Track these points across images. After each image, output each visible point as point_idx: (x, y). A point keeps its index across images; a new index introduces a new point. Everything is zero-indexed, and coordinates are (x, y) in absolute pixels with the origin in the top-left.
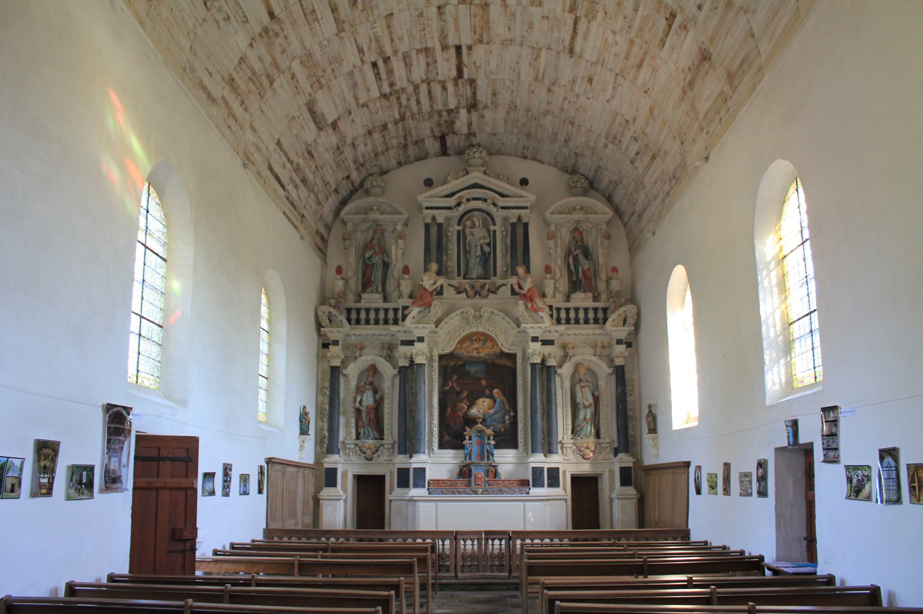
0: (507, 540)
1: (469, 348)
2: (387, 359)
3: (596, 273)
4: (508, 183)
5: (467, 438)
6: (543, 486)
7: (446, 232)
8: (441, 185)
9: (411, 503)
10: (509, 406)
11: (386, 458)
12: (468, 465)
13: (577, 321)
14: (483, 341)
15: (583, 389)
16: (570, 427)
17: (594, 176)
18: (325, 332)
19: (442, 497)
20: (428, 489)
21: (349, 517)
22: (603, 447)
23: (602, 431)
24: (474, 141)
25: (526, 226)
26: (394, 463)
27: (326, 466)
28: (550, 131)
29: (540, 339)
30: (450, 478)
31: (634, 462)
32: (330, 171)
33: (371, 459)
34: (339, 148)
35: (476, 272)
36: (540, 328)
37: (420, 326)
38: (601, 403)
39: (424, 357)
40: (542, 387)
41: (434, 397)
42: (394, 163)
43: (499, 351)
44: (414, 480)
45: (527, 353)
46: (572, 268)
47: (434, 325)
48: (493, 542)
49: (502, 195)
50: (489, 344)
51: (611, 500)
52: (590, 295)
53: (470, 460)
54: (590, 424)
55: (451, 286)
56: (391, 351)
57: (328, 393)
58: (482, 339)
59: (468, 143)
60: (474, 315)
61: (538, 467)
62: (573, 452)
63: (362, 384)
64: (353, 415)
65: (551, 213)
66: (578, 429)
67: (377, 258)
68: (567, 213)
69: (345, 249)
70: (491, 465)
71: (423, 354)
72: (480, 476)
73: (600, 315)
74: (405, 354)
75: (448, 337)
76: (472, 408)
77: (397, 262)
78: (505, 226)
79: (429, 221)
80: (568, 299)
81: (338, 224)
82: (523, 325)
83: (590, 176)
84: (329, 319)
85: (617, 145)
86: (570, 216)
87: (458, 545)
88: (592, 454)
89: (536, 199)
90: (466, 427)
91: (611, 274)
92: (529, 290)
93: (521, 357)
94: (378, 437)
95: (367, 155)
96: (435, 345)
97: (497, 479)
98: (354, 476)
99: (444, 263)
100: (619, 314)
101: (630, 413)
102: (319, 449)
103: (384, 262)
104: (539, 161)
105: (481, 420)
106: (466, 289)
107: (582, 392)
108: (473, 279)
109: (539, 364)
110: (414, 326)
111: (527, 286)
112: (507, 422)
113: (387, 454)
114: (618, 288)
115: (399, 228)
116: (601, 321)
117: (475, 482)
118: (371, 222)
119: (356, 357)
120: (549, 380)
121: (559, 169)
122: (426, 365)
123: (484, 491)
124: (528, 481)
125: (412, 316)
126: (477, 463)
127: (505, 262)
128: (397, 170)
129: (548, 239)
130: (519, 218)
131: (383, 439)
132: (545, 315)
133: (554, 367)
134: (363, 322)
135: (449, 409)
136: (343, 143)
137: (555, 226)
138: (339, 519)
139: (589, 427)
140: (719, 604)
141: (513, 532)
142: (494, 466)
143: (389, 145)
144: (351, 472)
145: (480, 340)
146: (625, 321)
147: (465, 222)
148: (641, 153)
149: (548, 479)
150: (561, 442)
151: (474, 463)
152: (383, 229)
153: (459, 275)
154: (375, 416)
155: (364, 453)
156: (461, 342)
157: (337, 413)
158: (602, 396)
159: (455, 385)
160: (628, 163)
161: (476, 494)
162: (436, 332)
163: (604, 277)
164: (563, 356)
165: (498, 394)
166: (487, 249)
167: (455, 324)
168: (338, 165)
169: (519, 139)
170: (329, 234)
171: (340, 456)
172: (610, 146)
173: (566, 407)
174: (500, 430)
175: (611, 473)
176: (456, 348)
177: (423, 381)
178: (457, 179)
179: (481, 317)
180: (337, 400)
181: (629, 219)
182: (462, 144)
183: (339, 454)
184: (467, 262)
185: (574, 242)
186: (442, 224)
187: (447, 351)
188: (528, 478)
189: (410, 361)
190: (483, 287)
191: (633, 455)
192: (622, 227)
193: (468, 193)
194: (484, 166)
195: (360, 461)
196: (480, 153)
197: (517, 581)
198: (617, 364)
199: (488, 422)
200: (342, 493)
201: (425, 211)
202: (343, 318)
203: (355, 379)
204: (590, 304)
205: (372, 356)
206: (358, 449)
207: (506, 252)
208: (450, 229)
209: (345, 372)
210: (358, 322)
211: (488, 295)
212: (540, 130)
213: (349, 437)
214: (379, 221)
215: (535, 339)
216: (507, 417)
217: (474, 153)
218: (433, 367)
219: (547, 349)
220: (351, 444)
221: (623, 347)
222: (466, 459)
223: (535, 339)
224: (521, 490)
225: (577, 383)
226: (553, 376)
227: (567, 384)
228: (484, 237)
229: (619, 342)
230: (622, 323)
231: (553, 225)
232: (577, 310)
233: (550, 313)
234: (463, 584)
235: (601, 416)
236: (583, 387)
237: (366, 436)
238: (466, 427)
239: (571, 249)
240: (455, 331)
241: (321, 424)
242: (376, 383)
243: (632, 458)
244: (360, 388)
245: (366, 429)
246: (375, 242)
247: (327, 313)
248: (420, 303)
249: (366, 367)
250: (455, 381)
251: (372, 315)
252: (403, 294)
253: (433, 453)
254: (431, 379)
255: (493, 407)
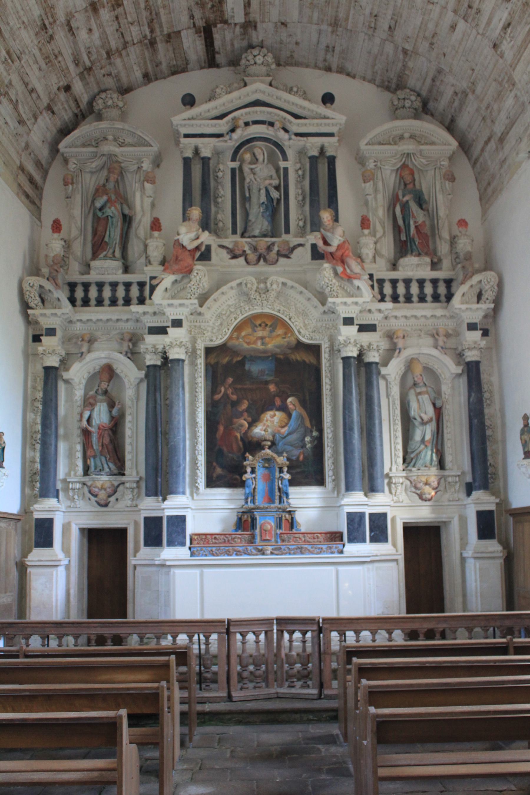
0: (316, 633)
1: (251, 337)
2: (129, 355)
3: (434, 228)
4: (305, 99)
5: (249, 470)
6: (364, 541)
7: (215, 171)
8: (206, 102)
9: (165, 570)
10: (311, 421)
11: (129, 503)
12: (250, 511)
13: (408, 299)
14: (271, 326)
15: (420, 397)
16: (401, 454)
17: (430, 91)
18: (34, 314)
19: (210, 560)
20: (190, 548)
21: (73, 591)
22: (449, 483)
23: (448, 458)
24: (256, 37)
25: (332, 161)
26: (139, 511)
27: (37, 515)
28: (367, 12)
29: (356, 322)
30: (224, 530)
31: (497, 504)
32: (35, 67)
33: (106, 505)
34: (44, 27)
35: (260, 227)
36: (356, 303)
37: (176, 302)
38: (446, 418)
39: (183, 350)
40: (360, 394)
41: (199, 410)
42: (138, 74)
43: (293, 341)
44: (169, 534)
45: (337, 343)
46: (400, 222)
47: (196, 301)
48: (291, 637)
49: (297, 117)
50: (280, 331)
51: (463, 560)
52: (428, 260)
53: (254, 503)
54: (430, 448)
55: (222, 247)
56: (135, 344)
57: (41, 407)
58: (269, 324)
59: (245, 43)
60: (258, 288)
61: (356, 513)
62: (406, 490)
63: (92, 393)
64: (79, 440)
65: (368, 144)
66: (412, 456)
67: (113, 208)
68: (390, 144)
69: (67, 198)
70: (284, 511)
71: (181, 345)
72: (269, 527)
73: (442, 290)
74: (154, 346)
75: (219, 322)
76: (256, 427)
77: (143, 215)
78: (300, 162)
79: (189, 154)
80: (394, 266)
81: (57, 165)
82: (330, 300)
83: (424, 93)
84: (40, 296)
85: (473, 19)
86: (395, 147)
87: (232, 642)
88: (433, 493)
89: (346, 121)
90: (247, 454)
91: (456, 231)
92: (339, 247)
93: (327, 350)
94: (116, 472)
95: (94, 51)
96: (199, 333)
97: (294, 531)
98: (82, 530)
99: (212, 217)
100: (472, 286)
101: (488, 432)
102: (27, 491)
103: (124, 216)
104: (348, 74)
105: (269, 443)
106: (244, 251)
107: (418, 401)
108: (254, 237)
109: (354, 358)
110: (165, 302)
111: (336, 241)
112: (308, 446)
113: (131, 496)
114: (469, 248)
115: (146, 165)
116: (443, 298)
117: (261, 536)
118: (104, 158)
119: (82, 354)
120: (369, 384)
121: (378, 86)
122: (186, 362)
123: (276, 549)
124: (341, 535)
125: (164, 288)
126: (264, 508)
127: (302, 214)
128: (144, 88)
129: (364, 182)
130: (322, 150)
131: (124, 475)
132: (363, 284)
133: (377, 364)
134: (93, 302)
135: (221, 428)
136: (51, 20)
137: (375, 161)
138: (57, 596)
139: (429, 453)
140: (516, 654)
141: (324, 620)
142: (289, 512)
143: (128, 38)
144: (76, 524)
145: (266, 325)
146: (479, 296)
147: (242, 154)
148: (513, 24)
149: (371, 530)
150: (387, 475)
151: (258, 508)
152: (122, 168)
153: (234, 232)
154: (111, 441)
155: (96, 496)
156: (238, 328)
157: (53, 437)
158: (448, 407)
159: (230, 391)
160: (488, 51)
161: (263, 554)
162: (200, 314)
163: (446, 235)
164: (388, 350)
165: (294, 405)
166: (275, 194)
167: (230, 303)
168: (47, 59)
169: (320, 32)
170: (44, 183)
171: (58, 501)
172: (461, 25)
173: (395, 424)
174: (298, 458)
175: (463, 520)
176: (230, 338)
177: (181, 385)
178: (230, 93)
179: (268, 291)
180: (53, 417)
181: (483, 150)
182: (237, 45)
183: (57, 497)
184: (246, 214)
185: (402, 186)
186: (209, 159)
187: (218, 342)
188: (341, 530)
189: (163, 358)
190: (269, 248)
191: (496, 493)
192: (469, 167)
193: (246, 114)
194: (269, 76)
195: (89, 508)
196: (264, 57)
197: (333, 704)
198: (468, 359)
199: (280, 446)
200: (61, 555)
201: (184, 141)
202: (63, 295)
203: (82, 386)
204: (427, 273)
205: (106, 352)
206: (86, 489)
207: (304, 199)
208: (221, 167)
209: (66, 375)
210: (86, 302)
211: (277, 260)
212: (352, 12)
213: (72, 473)
214: (116, 156)
215: (348, 321)
216: (308, 439)
217: (255, 56)
218: (197, 365)
219: (366, 338)
220: (76, 482)
221: (478, 334)
222: (247, 503)
223: (348, 321)
224: (331, 548)
225: (410, 388)
226: (375, 377)
227: (396, 391)
228: (271, 177)
229: (472, 327)
230: (475, 299)
231: (371, 161)
232: (407, 282)
233: (371, 283)
234: (241, 712)
235: (446, 436)
236: (420, 393)
237: (98, 470)
238: (247, 454)
239: (397, 195)
240: (228, 313)
241: (32, 454)
242: (113, 393)
243: (494, 498)
244: (89, 398)
245: (98, 460)
246: (111, 185)
247: (36, 287)
248: (176, 267)
249: (98, 368)
250: (230, 386)
251: (107, 293)
252: (152, 260)
253: (198, 494)
254: (193, 379)
255: (287, 424)
